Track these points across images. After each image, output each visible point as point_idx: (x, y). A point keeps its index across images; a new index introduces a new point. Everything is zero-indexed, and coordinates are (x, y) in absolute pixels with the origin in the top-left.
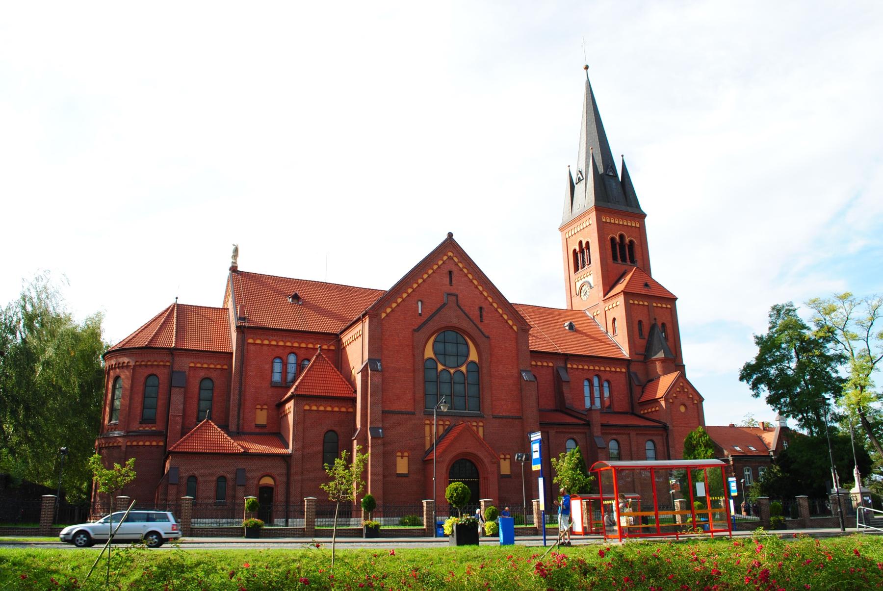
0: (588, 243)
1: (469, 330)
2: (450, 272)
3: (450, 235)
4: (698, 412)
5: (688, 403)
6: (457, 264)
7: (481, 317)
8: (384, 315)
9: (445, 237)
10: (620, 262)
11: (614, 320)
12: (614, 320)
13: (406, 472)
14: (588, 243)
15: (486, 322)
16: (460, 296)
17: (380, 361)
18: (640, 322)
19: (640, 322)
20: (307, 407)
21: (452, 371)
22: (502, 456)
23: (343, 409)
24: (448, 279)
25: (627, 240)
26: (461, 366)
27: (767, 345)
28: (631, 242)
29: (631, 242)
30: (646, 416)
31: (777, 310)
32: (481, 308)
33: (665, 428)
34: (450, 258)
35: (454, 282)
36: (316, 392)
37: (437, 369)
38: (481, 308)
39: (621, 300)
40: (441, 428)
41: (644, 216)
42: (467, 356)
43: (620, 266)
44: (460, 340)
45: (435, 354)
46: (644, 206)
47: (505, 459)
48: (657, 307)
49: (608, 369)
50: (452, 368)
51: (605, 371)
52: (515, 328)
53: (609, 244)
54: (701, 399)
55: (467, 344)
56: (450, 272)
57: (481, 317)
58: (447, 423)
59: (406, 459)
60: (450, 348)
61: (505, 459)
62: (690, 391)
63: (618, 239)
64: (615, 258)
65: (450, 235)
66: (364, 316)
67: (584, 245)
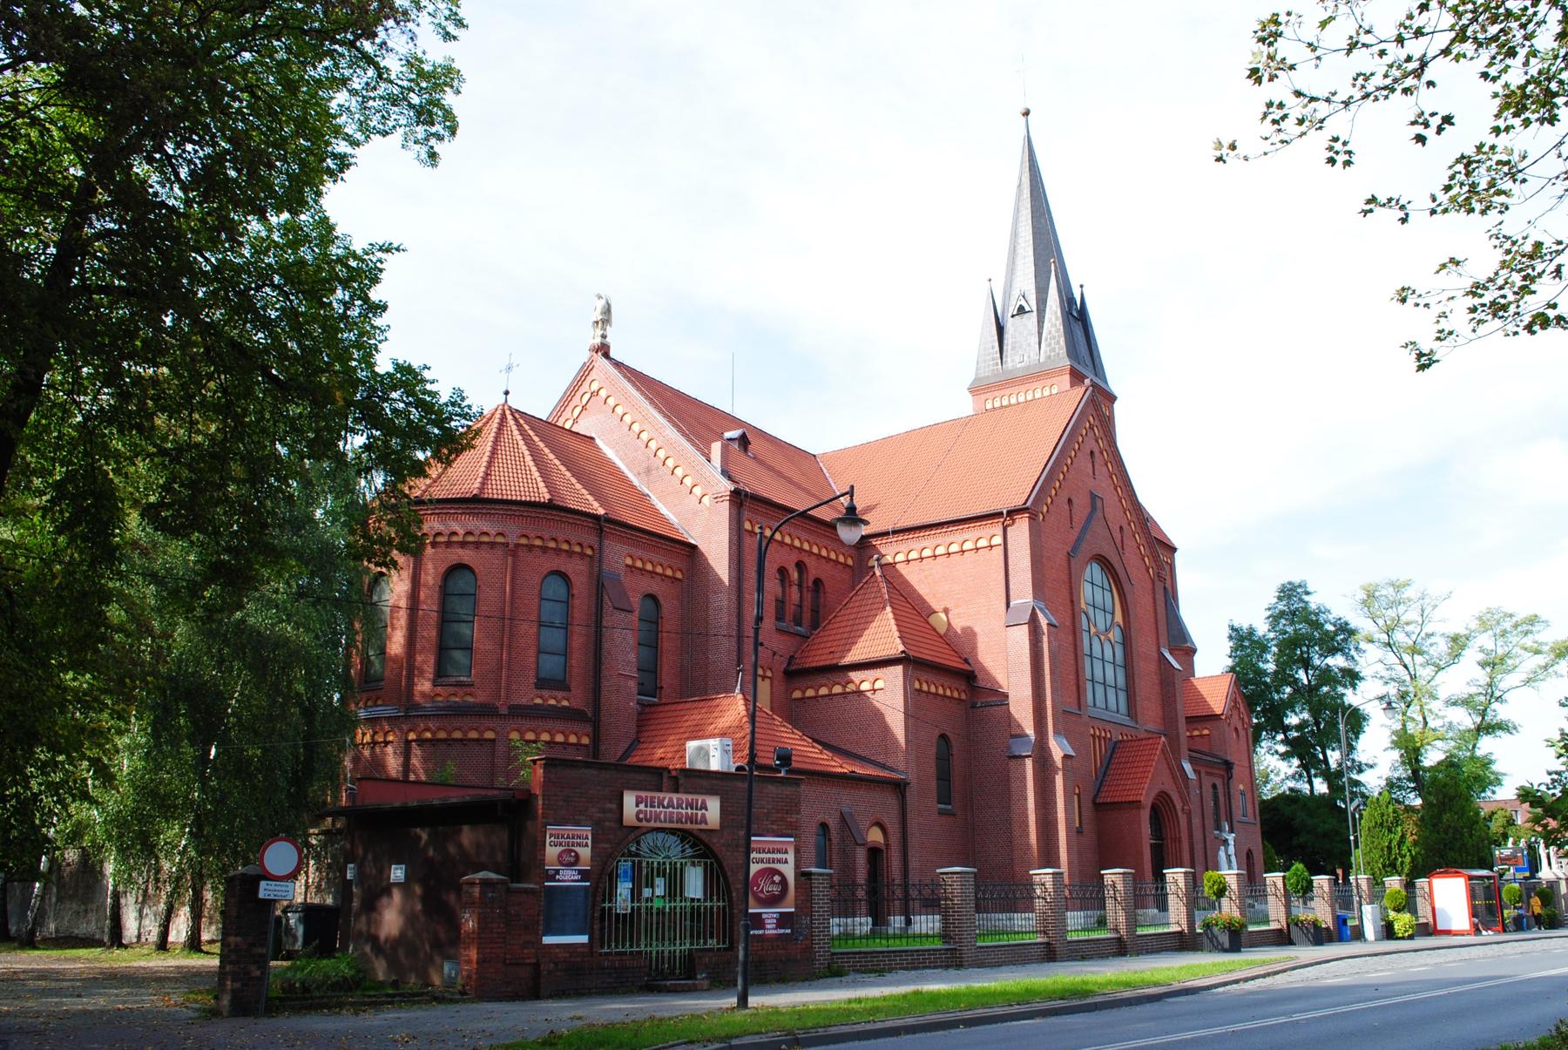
31: (1289, 592)
33: (1228, 766)
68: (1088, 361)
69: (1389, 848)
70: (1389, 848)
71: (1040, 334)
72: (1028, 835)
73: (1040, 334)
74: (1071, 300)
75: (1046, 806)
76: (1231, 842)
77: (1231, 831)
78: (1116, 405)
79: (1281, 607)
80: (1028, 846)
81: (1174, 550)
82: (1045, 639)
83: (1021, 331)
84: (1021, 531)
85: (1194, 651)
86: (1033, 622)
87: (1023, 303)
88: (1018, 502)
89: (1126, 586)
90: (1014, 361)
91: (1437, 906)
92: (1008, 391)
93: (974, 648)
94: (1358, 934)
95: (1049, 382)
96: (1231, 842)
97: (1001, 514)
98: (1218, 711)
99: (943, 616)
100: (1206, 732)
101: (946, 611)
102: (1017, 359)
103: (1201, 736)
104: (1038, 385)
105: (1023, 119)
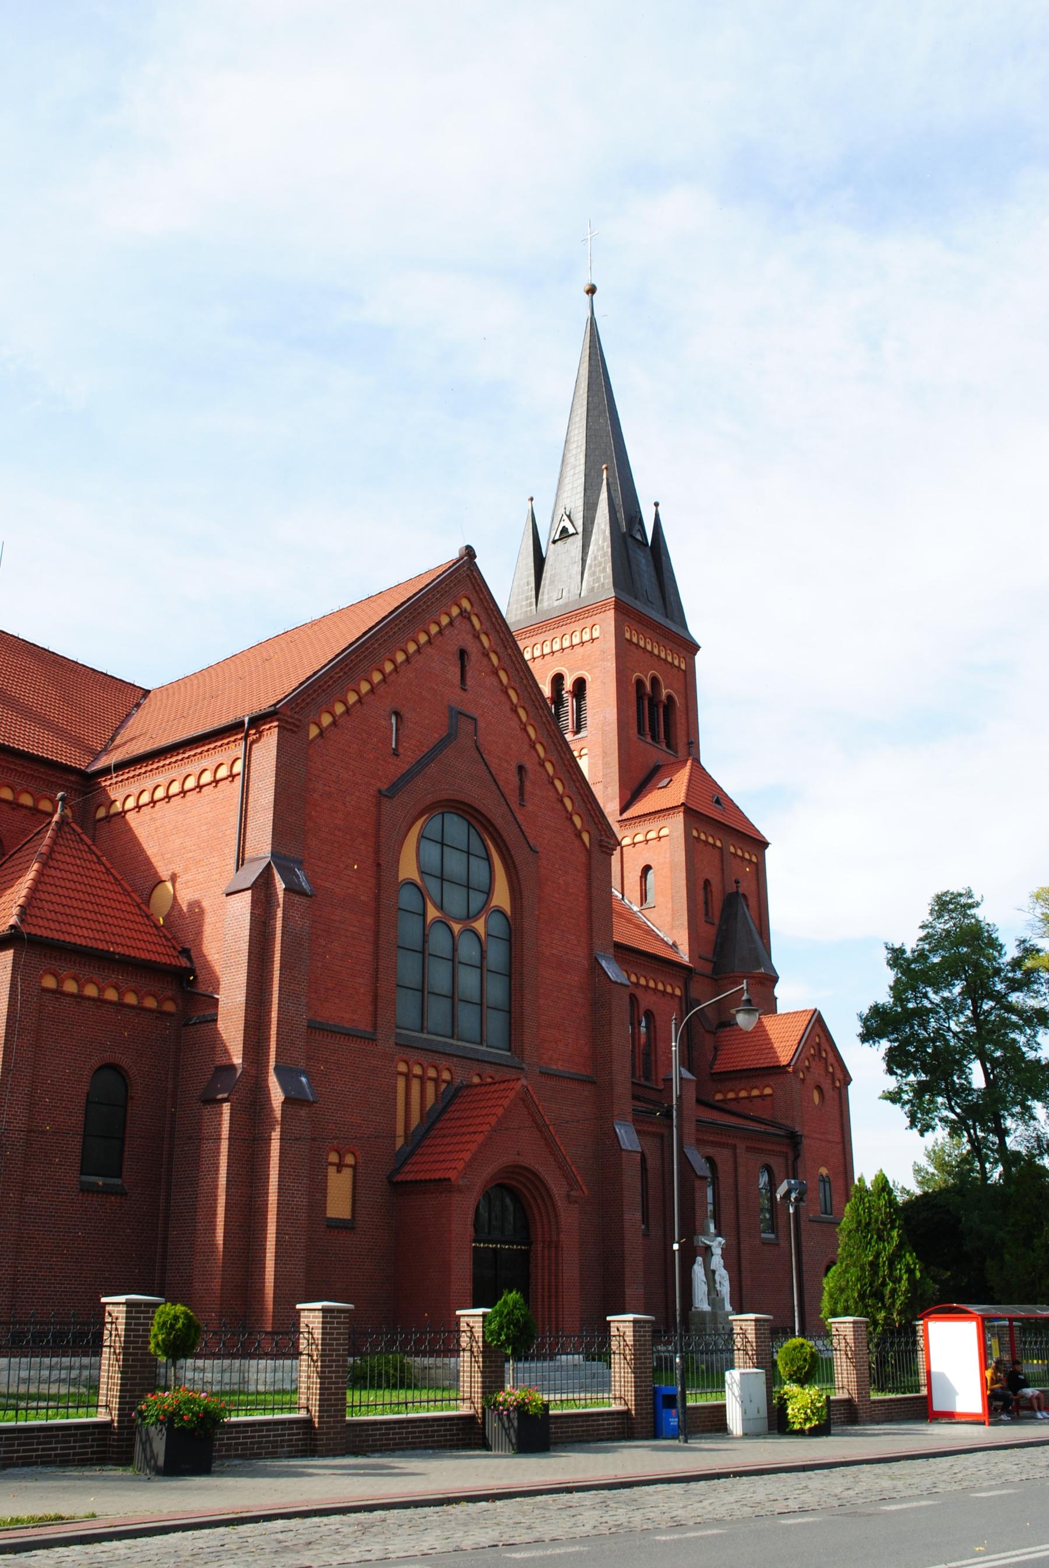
0: (580, 685)
1: (498, 822)
2: (463, 654)
3: (469, 553)
4: (841, 1106)
5: (826, 1086)
6: (477, 637)
7: (522, 788)
8: (314, 731)
9: (452, 553)
10: (649, 740)
11: (647, 869)
12: (647, 869)
13: (347, 1215)
14: (580, 685)
15: (530, 807)
16: (482, 724)
17: (300, 864)
18: (707, 883)
19: (707, 883)
20: (49, 982)
21: (457, 928)
22: (333, 1158)
23: (150, 1003)
24: (458, 671)
25: (664, 692)
26: (476, 917)
27: (910, 971)
28: (670, 697)
29: (670, 697)
30: (732, 1107)
31: (944, 904)
32: (521, 769)
33: (794, 1140)
34: (464, 615)
35: (469, 682)
36: (80, 935)
37: (424, 915)
38: (521, 769)
39: (674, 827)
40: (430, 1087)
41: (694, 648)
42: (489, 893)
43: (658, 754)
44: (476, 846)
45: (422, 873)
46: (696, 629)
47: (340, 1167)
48: (735, 855)
49: (71, 987)
50: (458, 920)
51: (647, 987)
52: (586, 837)
53: (633, 690)
54: (847, 1079)
55: (489, 859)
56: (463, 654)
57: (522, 788)
58: (446, 1075)
59: (347, 1173)
60: (455, 864)
61: (340, 1167)
62: (831, 1059)
63: (648, 684)
64: (640, 731)
65: (469, 553)
66: (258, 721)
67: (568, 684)
68: (654, 594)
69: (874, 1265)
70: (874, 1265)
71: (584, 561)
72: (214, 1230)
73: (584, 561)
74: (635, 518)
75: (254, 1185)
76: (717, 1251)
77: (719, 1234)
78: (699, 658)
79: (940, 926)
80: (213, 1244)
81: (765, 844)
82: (280, 913)
83: (562, 559)
84: (267, 749)
85: (774, 979)
86: (262, 887)
87: (567, 523)
88: (264, 702)
89: (520, 855)
90: (553, 598)
91: (933, 1369)
92: (540, 638)
93: (199, 933)
94: (713, 1422)
95: (589, 621)
96: (717, 1251)
97: (241, 724)
98: (784, 1060)
99: (169, 885)
100: (768, 1091)
101: (174, 878)
102: (555, 595)
103: (762, 1097)
104: (577, 626)
105: (587, 297)
